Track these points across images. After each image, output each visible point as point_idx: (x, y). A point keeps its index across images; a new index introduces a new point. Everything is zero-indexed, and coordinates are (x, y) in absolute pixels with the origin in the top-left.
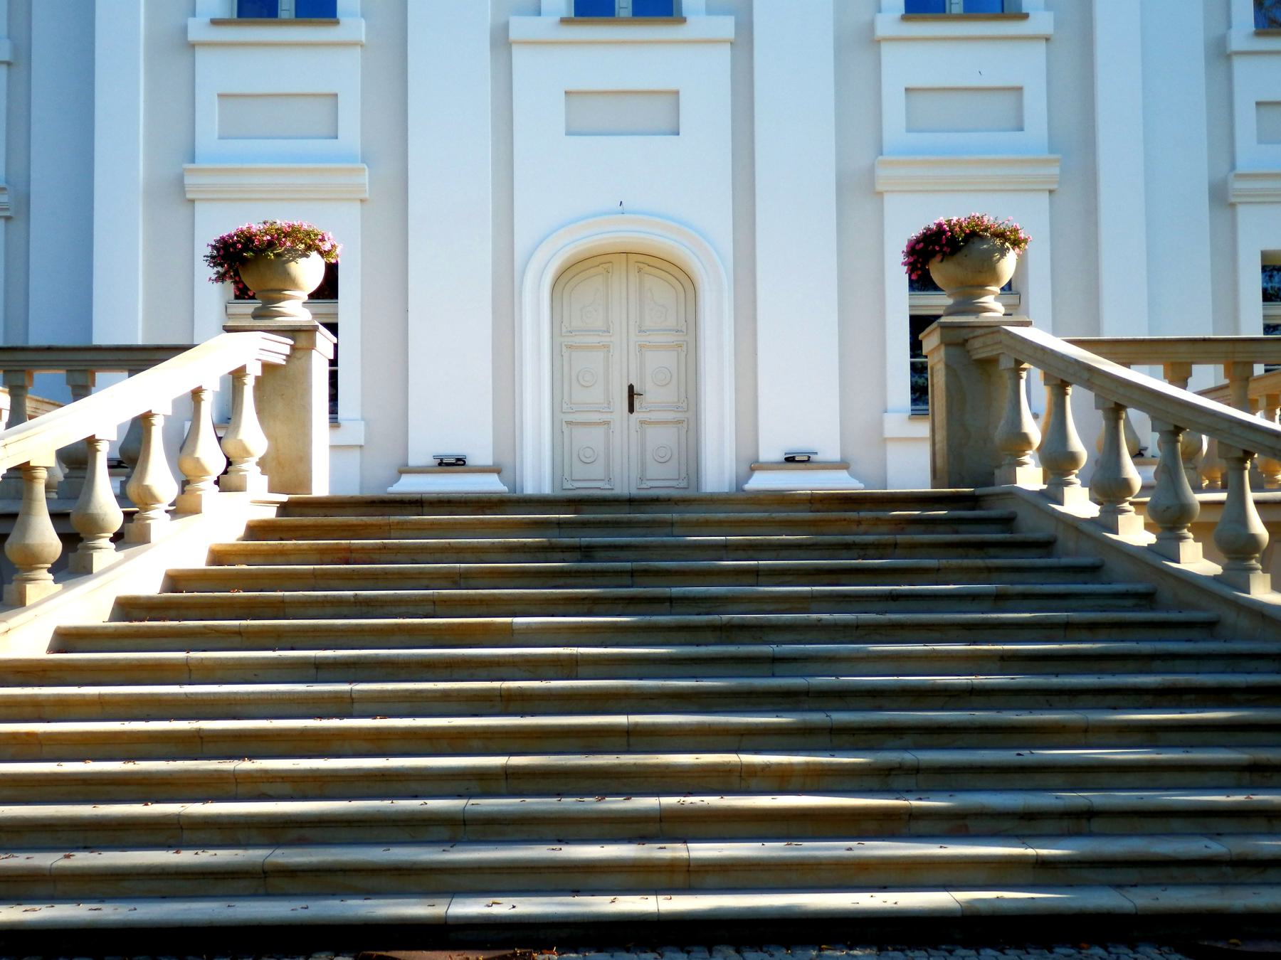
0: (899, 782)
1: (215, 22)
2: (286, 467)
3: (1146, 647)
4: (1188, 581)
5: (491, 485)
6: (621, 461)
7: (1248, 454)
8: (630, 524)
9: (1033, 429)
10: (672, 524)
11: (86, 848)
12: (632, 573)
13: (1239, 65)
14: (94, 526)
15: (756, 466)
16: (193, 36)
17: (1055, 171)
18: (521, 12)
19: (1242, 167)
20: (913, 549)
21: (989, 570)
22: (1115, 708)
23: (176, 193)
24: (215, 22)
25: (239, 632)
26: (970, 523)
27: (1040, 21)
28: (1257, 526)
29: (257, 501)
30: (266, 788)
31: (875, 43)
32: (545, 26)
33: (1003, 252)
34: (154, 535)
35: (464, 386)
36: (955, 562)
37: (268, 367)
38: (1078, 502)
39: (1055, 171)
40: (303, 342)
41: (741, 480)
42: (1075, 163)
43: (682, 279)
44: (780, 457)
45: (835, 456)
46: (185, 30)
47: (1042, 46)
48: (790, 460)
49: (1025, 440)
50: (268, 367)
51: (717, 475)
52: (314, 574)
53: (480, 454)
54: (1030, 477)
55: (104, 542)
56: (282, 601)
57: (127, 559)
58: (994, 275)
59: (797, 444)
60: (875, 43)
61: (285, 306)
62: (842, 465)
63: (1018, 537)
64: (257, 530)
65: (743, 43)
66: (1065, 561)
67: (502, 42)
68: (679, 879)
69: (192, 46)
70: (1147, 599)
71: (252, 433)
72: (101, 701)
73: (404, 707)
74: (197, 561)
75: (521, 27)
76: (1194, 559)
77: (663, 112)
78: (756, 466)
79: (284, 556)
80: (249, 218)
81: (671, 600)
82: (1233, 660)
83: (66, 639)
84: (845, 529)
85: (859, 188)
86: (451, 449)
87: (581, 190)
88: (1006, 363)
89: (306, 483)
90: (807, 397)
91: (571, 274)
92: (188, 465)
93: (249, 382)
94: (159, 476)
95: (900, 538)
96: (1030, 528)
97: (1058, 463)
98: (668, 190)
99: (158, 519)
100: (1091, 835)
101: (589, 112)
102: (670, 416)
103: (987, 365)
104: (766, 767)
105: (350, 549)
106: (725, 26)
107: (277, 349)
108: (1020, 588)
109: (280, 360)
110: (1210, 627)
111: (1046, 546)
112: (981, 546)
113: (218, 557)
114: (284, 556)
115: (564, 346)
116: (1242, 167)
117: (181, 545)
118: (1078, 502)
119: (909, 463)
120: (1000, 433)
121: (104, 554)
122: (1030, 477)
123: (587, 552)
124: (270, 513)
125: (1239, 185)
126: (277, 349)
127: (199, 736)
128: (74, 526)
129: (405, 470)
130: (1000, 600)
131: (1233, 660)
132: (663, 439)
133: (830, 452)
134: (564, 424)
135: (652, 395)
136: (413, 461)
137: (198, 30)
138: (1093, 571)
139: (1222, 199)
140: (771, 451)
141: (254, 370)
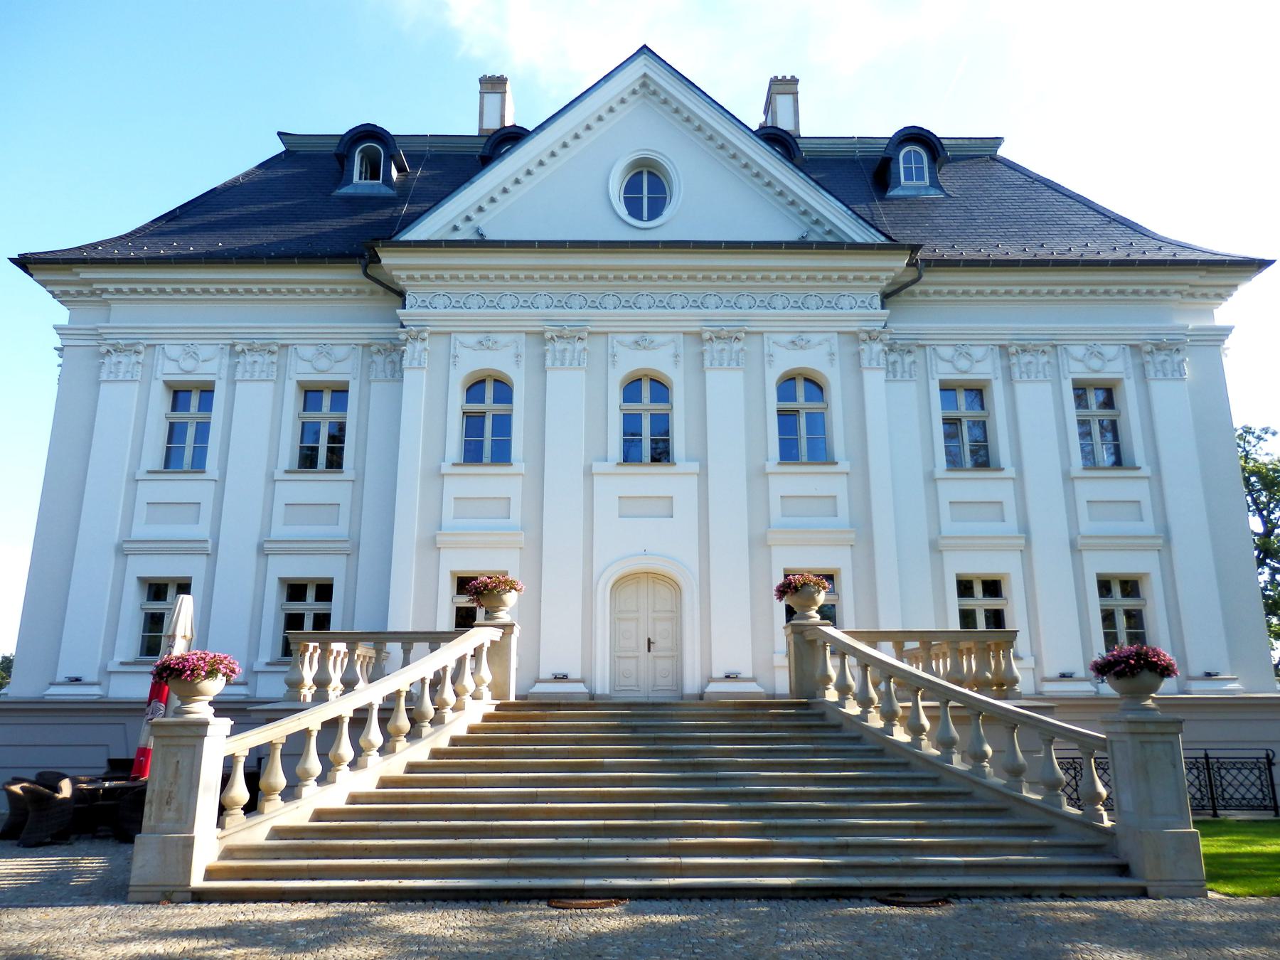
0: (769, 832)
1: (454, 465)
2: (498, 689)
3: (877, 774)
4: (897, 744)
5: (580, 688)
6: (644, 679)
7: (919, 689)
8: (653, 715)
9: (833, 673)
10: (672, 715)
11: (432, 857)
12: (655, 739)
13: (940, 485)
14: (422, 717)
15: (711, 679)
16: (443, 471)
17: (853, 536)
18: (597, 460)
19: (944, 533)
20: (778, 728)
21: (812, 738)
22: (862, 801)
23: (432, 545)
24: (454, 465)
25: (485, 765)
26: (798, 720)
27: (843, 466)
28: (925, 722)
29: (488, 705)
30: (504, 833)
31: (766, 475)
32: (610, 466)
33: (819, 592)
34: (447, 720)
35: (565, 638)
36: (797, 735)
37: (493, 642)
38: (853, 709)
39: (853, 536)
40: (508, 630)
41: (704, 687)
42: (862, 534)
43: (674, 586)
44: (723, 675)
45: (750, 675)
46: (440, 467)
47: (844, 478)
48: (727, 677)
49: (829, 679)
50: (493, 642)
51: (692, 685)
52: (515, 738)
53: (575, 673)
54: (832, 695)
55: (426, 724)
56: (503, 751)
57: (436, 731)
58: (814, 602)
59: (731, 669)
60: (766, 475)
61: (500, 614)
62: (753, 680)
63: (825, 723)
64: (487, 718)
65: (703, 475)
66: (846, 734)
67: (589, 473)
68: (677, 872)
69: (443, 475)
70: (880, 752)
71: (486, 673)
72: (431, 795)
73: (398, 834)
74: (463, 732)
75: (598, 467)
76: (900, 735)
77: (666, 507)
78: (711, 679)
79: (500, 730)
80: (477, 563)
81: (672, 751)
82: (914, 780)
83: (412, 768)
84: (748, 716)
85: (759, 543)
86: (561, 670)
87: (626, 544)
88: (820, 643)
89: (507, 697)
90: (737, 650)
91: (621, 583)
92: (459, 689)
93: (485, 649)
94: (448, 693)
95: (774, 723)
96: (832, 719)
97: (843, 689)
98: (668, 544)
99: (448, 714)
100: (848, 855)
101: (630, 506)
102: (668, 654)
103: (813, 642)
104: (713, 825)
105: (529, 727)
106: (695, 467)
107: (496, 634)
108: (824, 747)
109: (498, 639)
110: (906, 765)
111: (838, 727)
112: (810, 727)
113: (472, 730)
114: (500, 730)
115: (617, 617)
116: (944, 533)
117: (458, 724)
118: (853, 709)
119: (782, 683)
120: (818, 673)
121: (427, 729)
122: (832, 695)
123: (634, 729)
124: (492, 710)
125: (943, 542)
126: (496, 634)
127: (475, 810)
128: (414, 715)
129: (538, 681)
130: (816, 753)
131: (914, 780)
132: (664, 665)
133: (747, 673)
134: (615, 658)
135: (661, 643)
136: (542, 676)
137: (446, 468)
138: (857, 739)
139: (936, 548)
140: (718, 672)
141: (487, 644)
